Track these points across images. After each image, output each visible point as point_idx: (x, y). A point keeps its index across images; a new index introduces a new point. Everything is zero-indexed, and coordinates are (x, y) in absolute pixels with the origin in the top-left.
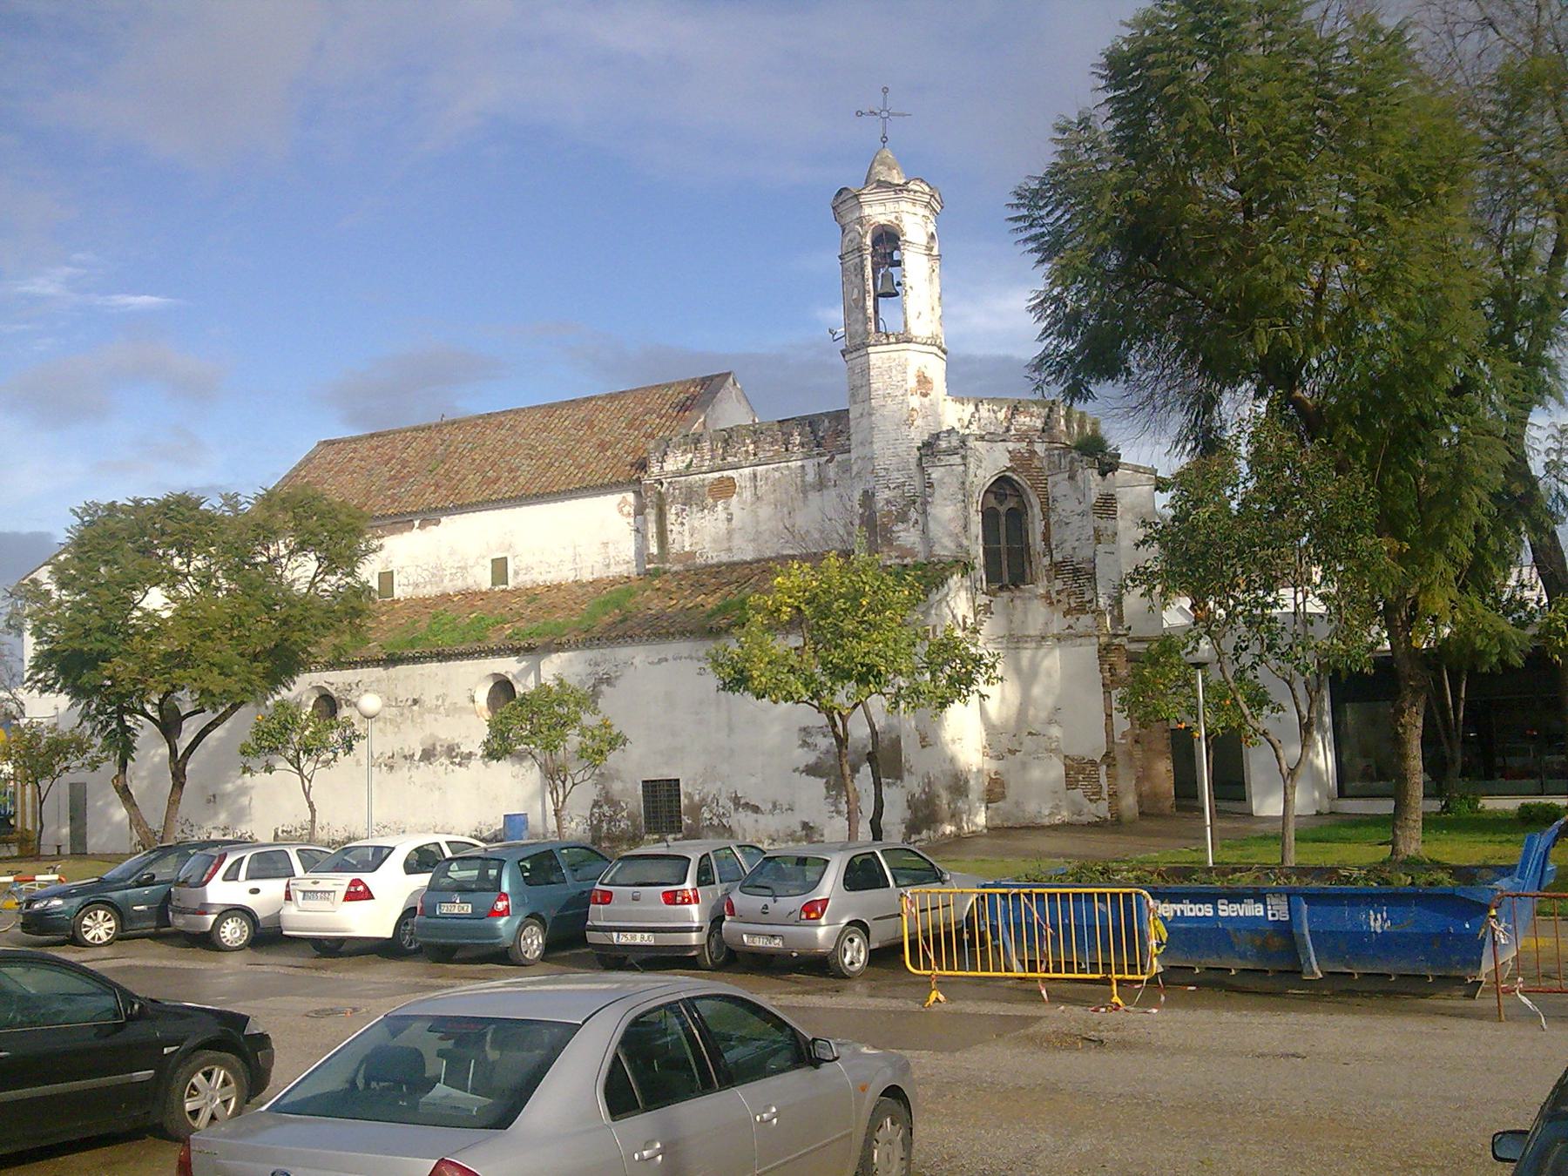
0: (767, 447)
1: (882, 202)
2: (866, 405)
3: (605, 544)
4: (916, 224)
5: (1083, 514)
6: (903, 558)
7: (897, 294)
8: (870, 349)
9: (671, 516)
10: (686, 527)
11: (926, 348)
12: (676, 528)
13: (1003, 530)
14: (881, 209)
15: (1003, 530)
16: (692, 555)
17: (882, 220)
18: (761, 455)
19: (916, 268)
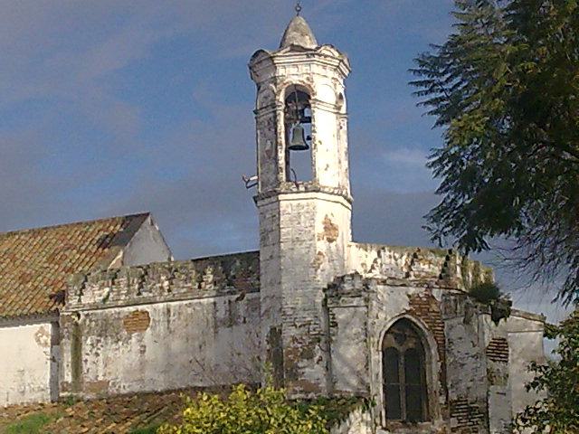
0: (181, 284)
2: (276, 249)
3: (22, 372)
4: (326, 84)
5: (476, 357)
6: (307, 393)
7: (307, 147)
9: (86, 347)
10: (101, 357)
12: (91, 358)
13: (403, 399)
14: (293, 70)
15: (403, 399)
16: (105, 384)
17: (295, 80)
18: (145, 294)
19: (328, 130)
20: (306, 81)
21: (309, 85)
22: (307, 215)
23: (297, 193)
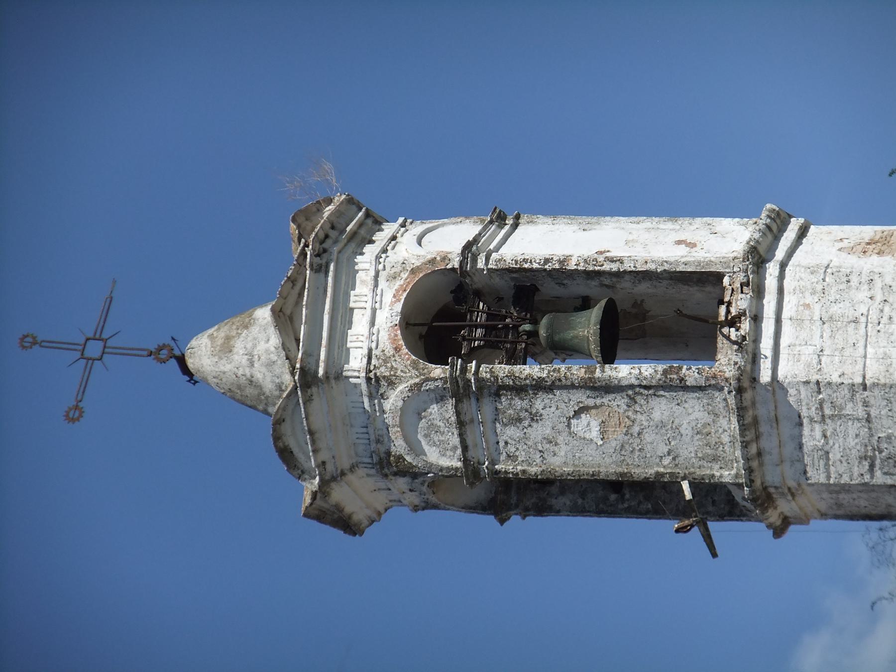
1: (343, 317)
8: (765, 376)
11: (771, 283)
17: (390, 313)
20: (398, 283)
21: (413, 271)
22: (833, 294)
23: (757, 319)
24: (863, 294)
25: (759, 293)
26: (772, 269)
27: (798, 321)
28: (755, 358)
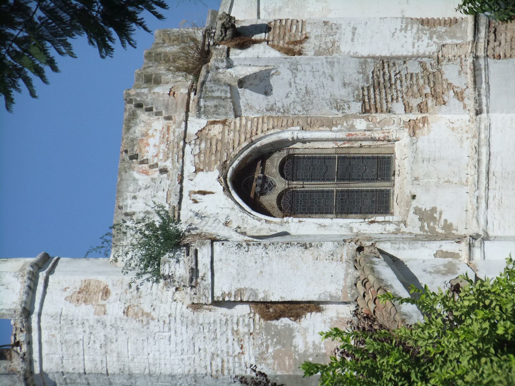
5: (294, 69)
8: (37, 371)
23: (29, 343)
24: (80, 330)
25: (29, 330)
26: (34, 318)
27: (50, 343)
28: (31, 362)
